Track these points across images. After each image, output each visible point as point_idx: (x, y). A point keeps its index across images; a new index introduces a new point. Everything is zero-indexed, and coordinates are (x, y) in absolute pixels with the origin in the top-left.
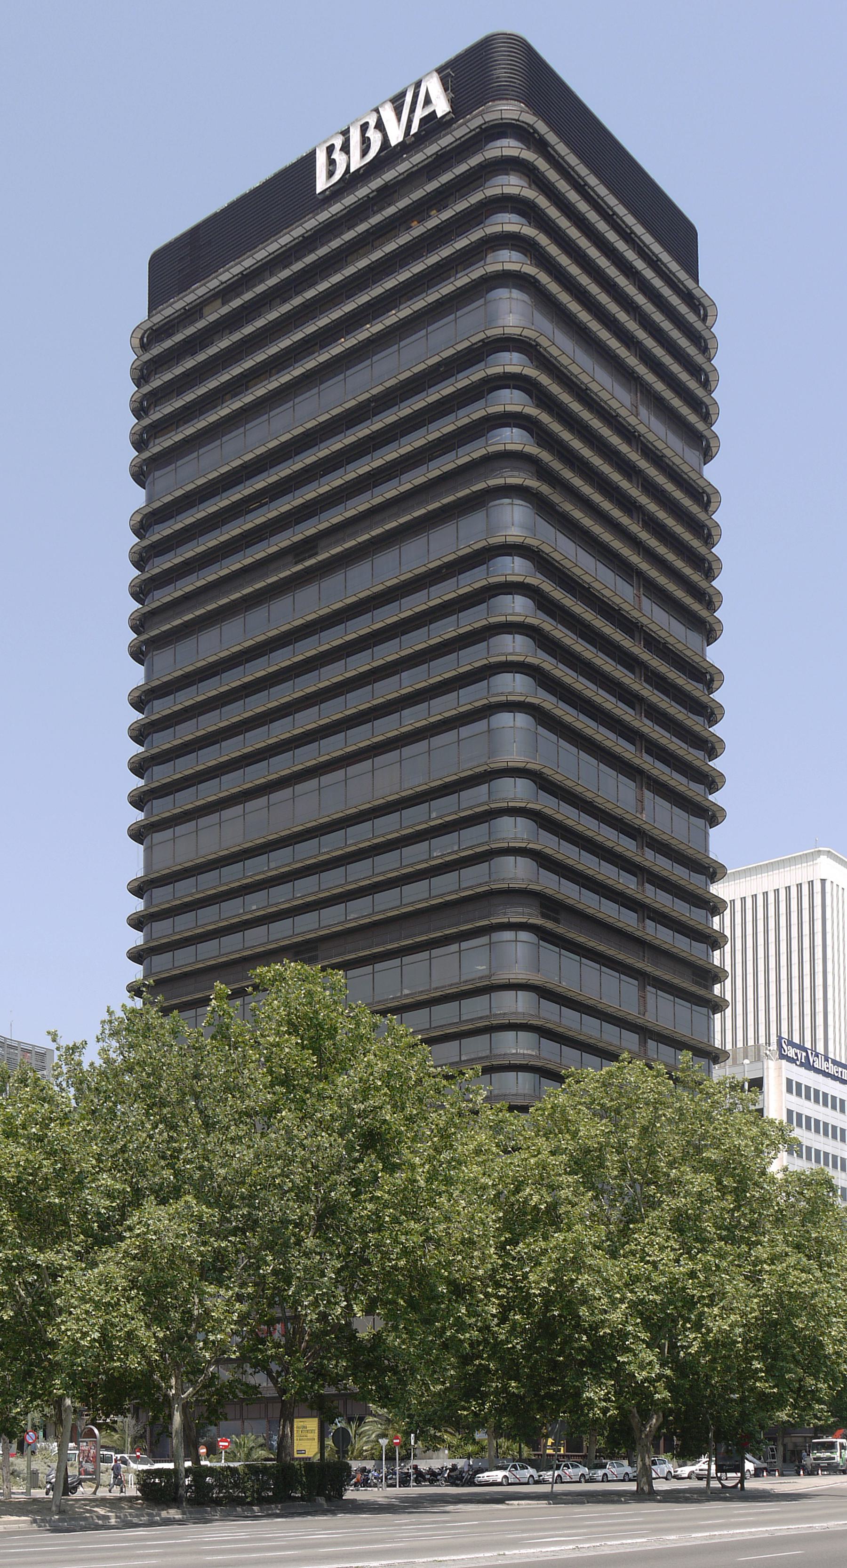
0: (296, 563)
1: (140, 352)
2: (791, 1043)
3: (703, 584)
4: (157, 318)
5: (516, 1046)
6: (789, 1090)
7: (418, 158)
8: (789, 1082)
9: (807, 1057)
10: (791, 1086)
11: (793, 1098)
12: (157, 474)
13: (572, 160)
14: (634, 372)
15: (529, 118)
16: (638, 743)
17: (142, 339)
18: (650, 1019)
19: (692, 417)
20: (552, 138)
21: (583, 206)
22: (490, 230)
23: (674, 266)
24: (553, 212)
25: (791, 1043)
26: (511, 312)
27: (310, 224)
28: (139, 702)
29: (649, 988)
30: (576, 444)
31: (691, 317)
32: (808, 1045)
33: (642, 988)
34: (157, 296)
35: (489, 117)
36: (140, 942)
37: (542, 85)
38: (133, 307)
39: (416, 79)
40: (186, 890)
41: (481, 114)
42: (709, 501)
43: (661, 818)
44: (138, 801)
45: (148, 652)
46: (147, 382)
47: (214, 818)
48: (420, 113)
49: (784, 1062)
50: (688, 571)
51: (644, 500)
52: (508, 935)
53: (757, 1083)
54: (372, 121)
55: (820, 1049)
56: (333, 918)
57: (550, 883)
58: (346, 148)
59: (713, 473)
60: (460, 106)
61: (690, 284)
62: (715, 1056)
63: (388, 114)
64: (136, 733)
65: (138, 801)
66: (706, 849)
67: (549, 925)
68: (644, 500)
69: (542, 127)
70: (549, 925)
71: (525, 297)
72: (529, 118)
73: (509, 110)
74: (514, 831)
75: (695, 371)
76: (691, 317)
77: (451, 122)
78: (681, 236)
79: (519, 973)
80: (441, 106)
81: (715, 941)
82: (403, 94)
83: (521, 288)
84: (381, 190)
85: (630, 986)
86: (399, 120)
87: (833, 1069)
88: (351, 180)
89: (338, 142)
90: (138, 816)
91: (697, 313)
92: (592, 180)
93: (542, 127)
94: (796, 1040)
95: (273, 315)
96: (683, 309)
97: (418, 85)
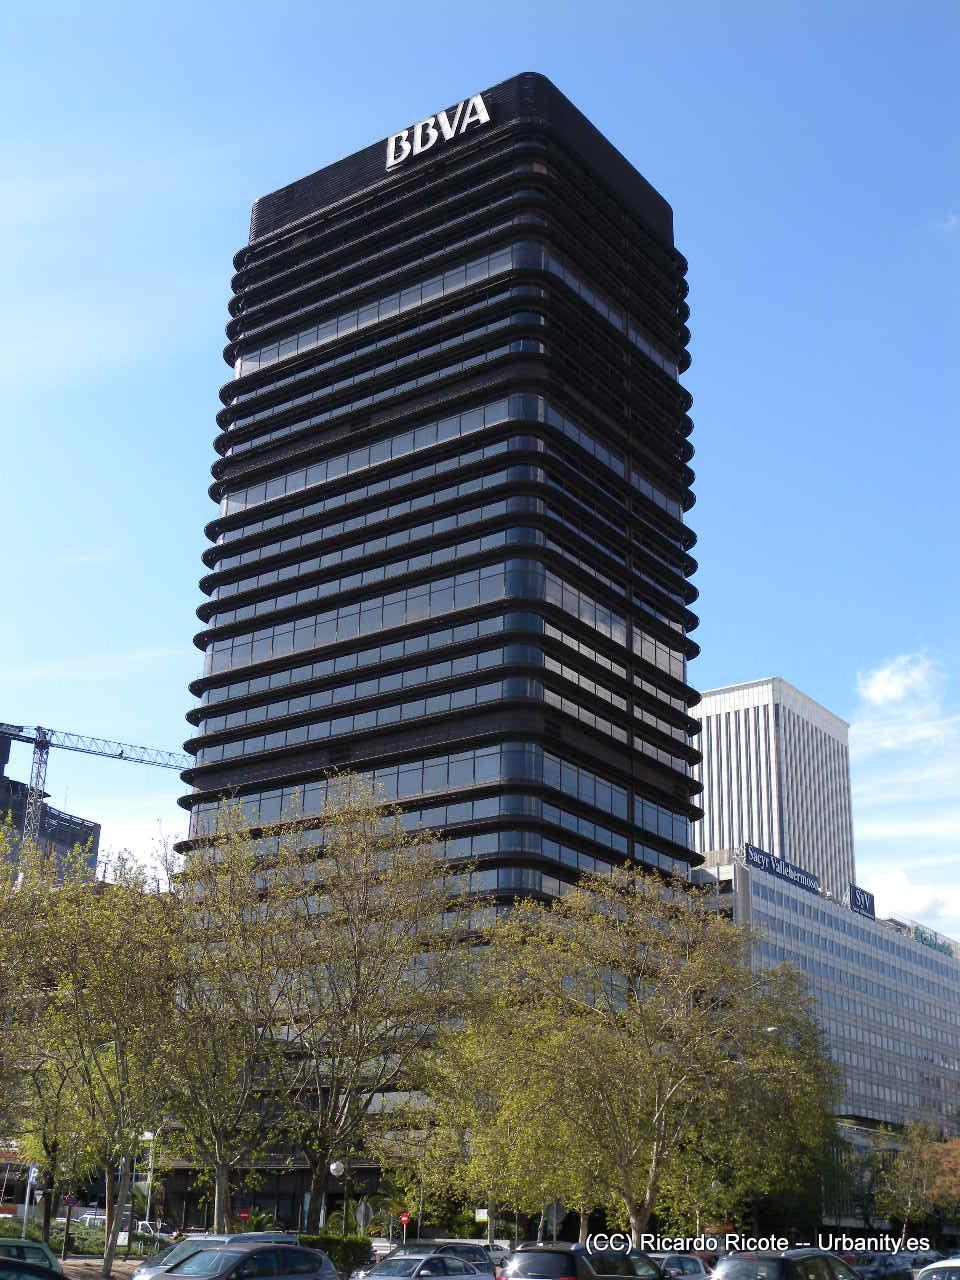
25: (759, 851)
40: (239, 690)
43: (649, 649)
48: (468, 120)
54: (432, 122)
58: (410, 139)
59: (685, 380)
63: (443, 119)
80: (484, 117)
81: (695, 757)
88: (412, 159)
89: (405, 134)
97: (466, 103)
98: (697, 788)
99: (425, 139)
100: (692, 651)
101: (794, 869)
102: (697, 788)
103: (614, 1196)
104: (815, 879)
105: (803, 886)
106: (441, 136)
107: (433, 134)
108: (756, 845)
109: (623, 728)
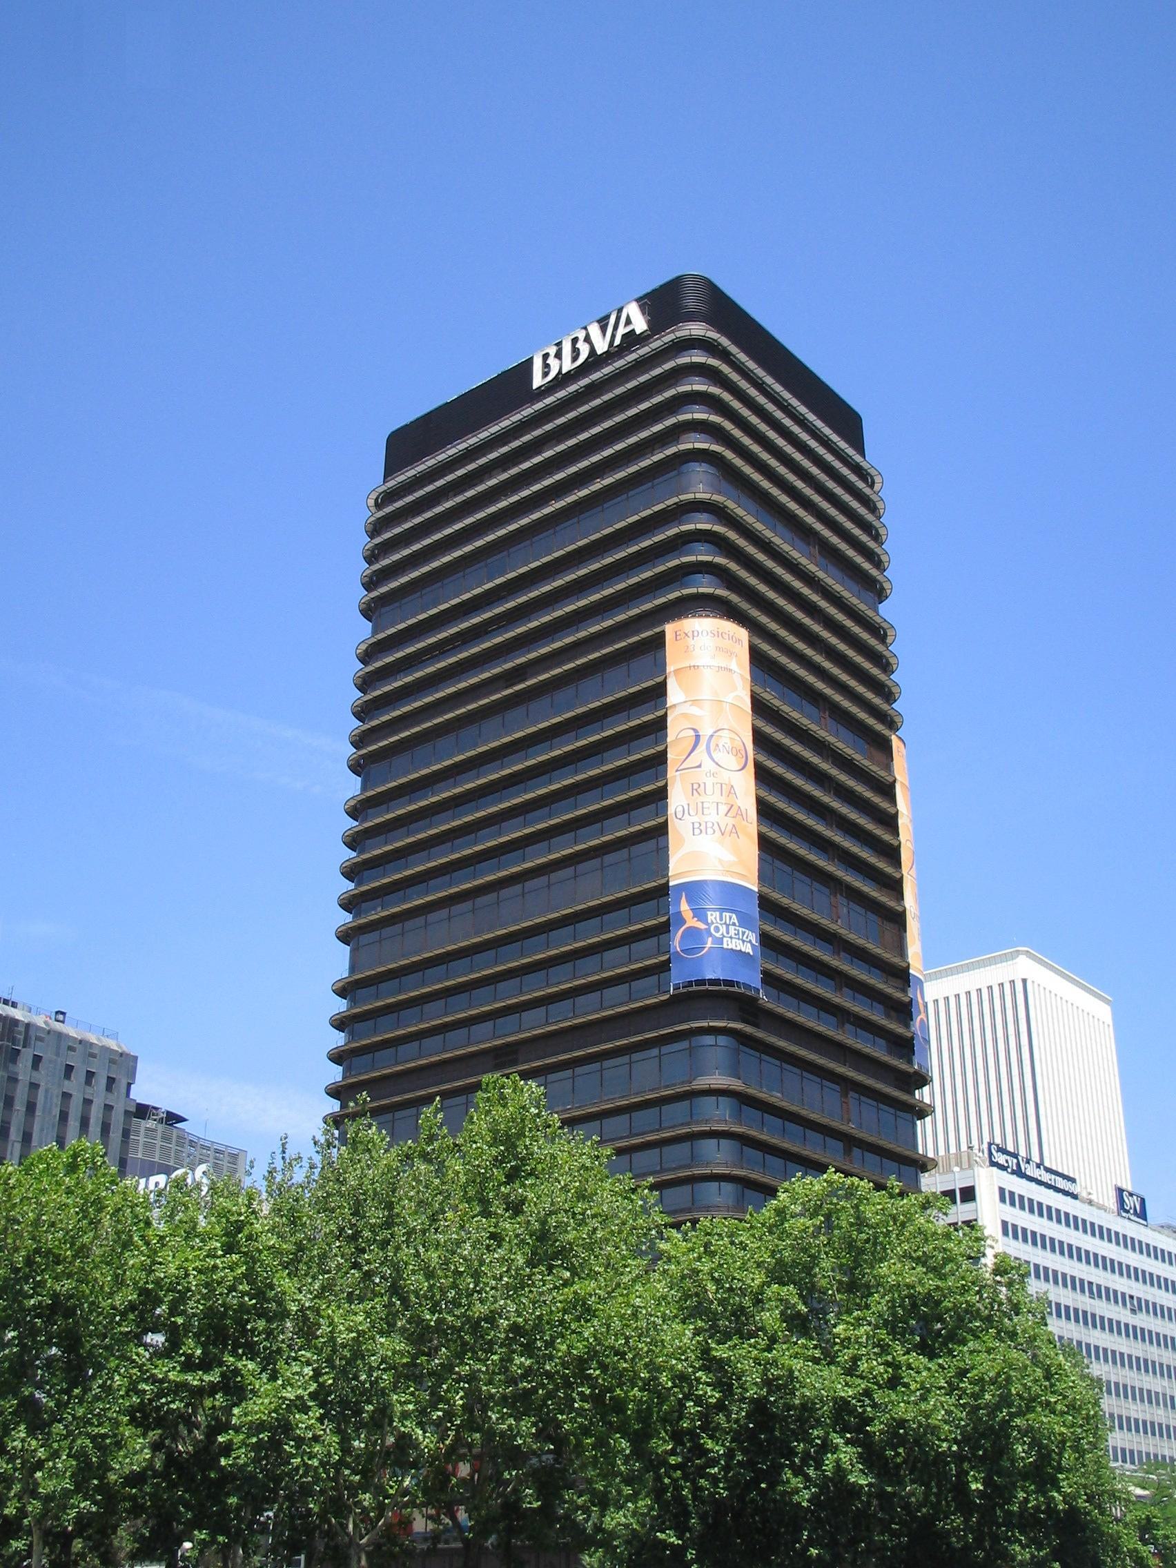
0: (507, 688)
1: (373, 509)
2: (1003, 1151)
3: (885, 707)
4: (391, 484)
5: (718, 1157)
6: (1003, 1200)
7: (620, 363)
8: (1002, 1190)
9: (1018, 1165)
10: (1005, 1196)
11: (1007, 1207)
12: (384, 610)
13: (751, 365)
14: (812, 528)
15: (713, 335)
17: (376, 500)
18: (851, 1128)
20: (733, 349)
21: (762, 400)
22: (682, 447)
23: (843, 445)
24: (736, 404)
25: (1003, 1151)
26: (700, 485)
27: (528, 411)
28: (354, 812)
29: (851, 1094)
30: (762, 588)
31: (860, 485)
33: (845, 1094)
34: (392, 465)
35: (679, 334)
36: (341, 1042)
37: (722, 310)
38: (370, 474)
39: (619, 306)
41: (673, 332)
42: (886, 635)
44: (350, 872)
45: (376, 607)
46: (377, 561)
47: (420, 921)
48: (622, 330)
49: (995, 1169)
50: (869, 695)
51: (825, 634)
52: (709, 1040)
53: (968, 1194)
54: (581, 335)
56: (534, 1025)
58: (558, 355)
59: (887, 611)
60: (656, 326)
61: (858, 458)
62: (923, 1165)
63: (594, 330)
64: (359, 681)
65: (350, 872)
67: (749, 1029)
68: (825, 634)
69: (725, 341)
70: (749, 1029)
71: (712, 470)
72: (713, 335)
73: (697, 329)
74: (719, 1115)
75: (867, 527)
76: (860, 485)
77: (649, 337)
78: (848, 422)
79: (718, 1080)
82: (608, 317)
83: (710, 463)
85: (832, 1094)
86: (604, 335)
87: (1046, 1177)
88: (563, 379)
89: (552, 351)
91: (870, 534)
92: (769, 380)
93: (725, 341)
95: (492, 482)
96: (853, 478)
97: (620, 311)
99: (576, 353)
101: (1048, 1170)
103: (616, 1519)
104: (1073, 1180)
105: (1058, 1190)
106: (593, 351)
108: (998, 1140)
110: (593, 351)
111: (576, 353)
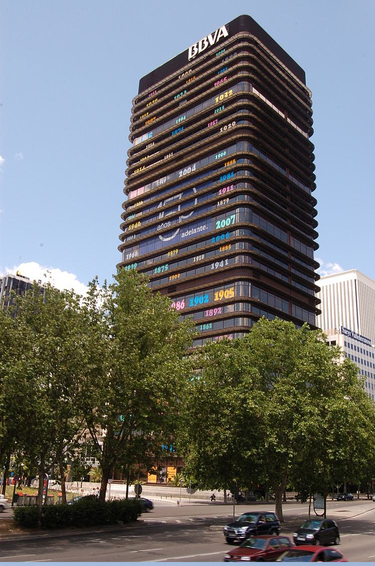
4: (140, 95)
9: (351, 334)
16: (288, 220)
19: (305, 118)
23: (298, 80)
25: (346, 329)
32: (352, 330)
38: (135, 92)
43: (295, 244)
44: (123, 238)
48: (219, 36)
54: (205, 39)
55: (356, 332)
57: (256, 265)
58: (197, 47)
61: (303, 85)
63: (210, 37)
66: (313, 257)
69: (256, 39)
78: (301, 74)
80: (226, 34)
84: (207, 57)
87: (361, 339)
88: (198, 55)
89: (195, 45)
90: (121, 243)
93: (256, 39)
94: (348, 329)
98: (319, 301)
99: (203, 45)
100: (316, 247)
102: (319, 301)
106: (209, 44)
107: (206, 44)
109: (287, 265)
110: (209, 44)
111: (203, 45)
